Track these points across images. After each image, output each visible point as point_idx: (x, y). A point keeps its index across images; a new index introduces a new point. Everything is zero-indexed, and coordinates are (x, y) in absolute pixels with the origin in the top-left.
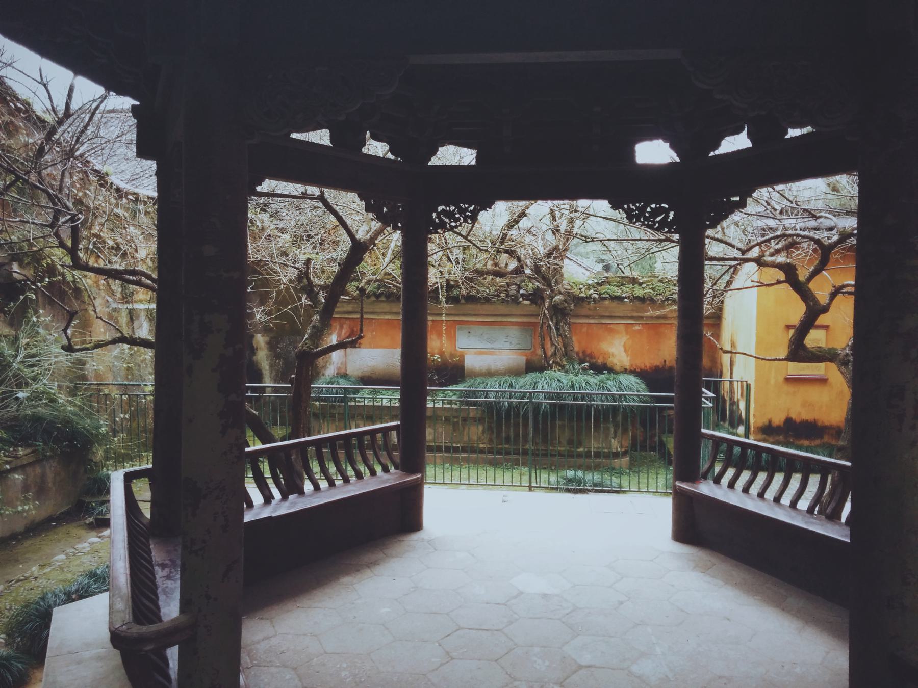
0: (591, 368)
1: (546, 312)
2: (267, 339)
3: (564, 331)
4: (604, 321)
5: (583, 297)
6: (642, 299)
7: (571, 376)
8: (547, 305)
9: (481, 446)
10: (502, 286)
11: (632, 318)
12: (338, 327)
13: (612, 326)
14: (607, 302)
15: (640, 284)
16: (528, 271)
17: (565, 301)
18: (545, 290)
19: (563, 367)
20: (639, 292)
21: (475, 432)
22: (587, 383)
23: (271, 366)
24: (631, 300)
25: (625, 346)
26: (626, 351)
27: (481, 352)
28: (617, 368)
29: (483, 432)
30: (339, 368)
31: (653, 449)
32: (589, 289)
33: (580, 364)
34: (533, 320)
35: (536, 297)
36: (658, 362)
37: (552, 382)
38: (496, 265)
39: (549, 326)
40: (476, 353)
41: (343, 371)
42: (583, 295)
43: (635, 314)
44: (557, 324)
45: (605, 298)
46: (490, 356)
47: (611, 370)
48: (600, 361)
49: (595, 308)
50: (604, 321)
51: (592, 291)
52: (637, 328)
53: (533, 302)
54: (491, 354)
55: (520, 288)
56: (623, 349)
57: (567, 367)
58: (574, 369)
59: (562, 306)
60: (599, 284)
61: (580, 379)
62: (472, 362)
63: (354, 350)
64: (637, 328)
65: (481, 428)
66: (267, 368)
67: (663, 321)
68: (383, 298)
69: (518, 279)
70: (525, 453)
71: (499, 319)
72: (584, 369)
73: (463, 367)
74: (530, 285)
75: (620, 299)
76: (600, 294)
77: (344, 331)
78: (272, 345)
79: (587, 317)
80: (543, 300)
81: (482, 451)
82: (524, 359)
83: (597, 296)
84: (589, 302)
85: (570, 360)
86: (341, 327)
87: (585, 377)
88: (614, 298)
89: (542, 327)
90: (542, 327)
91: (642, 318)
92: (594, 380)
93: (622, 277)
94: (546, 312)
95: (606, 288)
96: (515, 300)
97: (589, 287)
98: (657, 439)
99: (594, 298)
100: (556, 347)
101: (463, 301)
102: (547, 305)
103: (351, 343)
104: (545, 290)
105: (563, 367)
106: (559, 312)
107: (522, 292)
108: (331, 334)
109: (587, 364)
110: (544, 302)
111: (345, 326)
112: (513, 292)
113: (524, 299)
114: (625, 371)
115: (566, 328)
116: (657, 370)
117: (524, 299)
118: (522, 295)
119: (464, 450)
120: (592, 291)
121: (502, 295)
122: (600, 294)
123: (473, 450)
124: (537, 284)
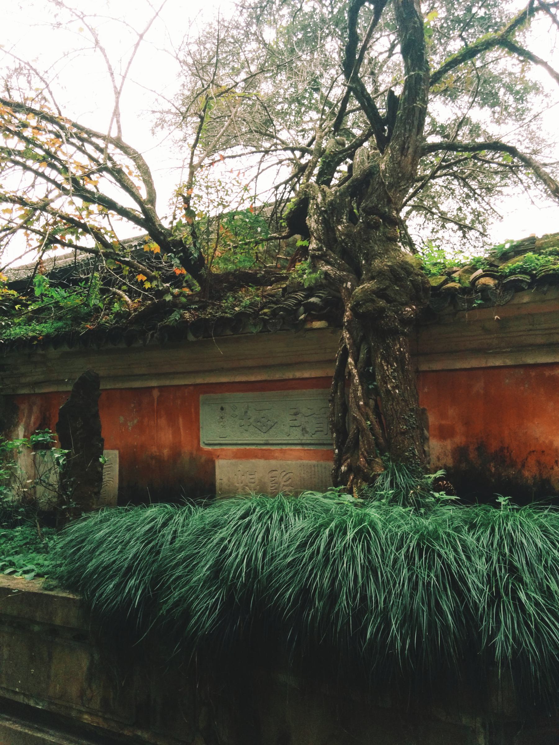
12: (26, 411)
17: (381, 293)
18: (342, 280)
46: (261, 462)
48: (529, 473)
54: (266, 455)
73: (213, 484)
77: (33, 420)
83: (490, 282)
99: (485, 287)
104: (342, 280)
108: (17, 425)
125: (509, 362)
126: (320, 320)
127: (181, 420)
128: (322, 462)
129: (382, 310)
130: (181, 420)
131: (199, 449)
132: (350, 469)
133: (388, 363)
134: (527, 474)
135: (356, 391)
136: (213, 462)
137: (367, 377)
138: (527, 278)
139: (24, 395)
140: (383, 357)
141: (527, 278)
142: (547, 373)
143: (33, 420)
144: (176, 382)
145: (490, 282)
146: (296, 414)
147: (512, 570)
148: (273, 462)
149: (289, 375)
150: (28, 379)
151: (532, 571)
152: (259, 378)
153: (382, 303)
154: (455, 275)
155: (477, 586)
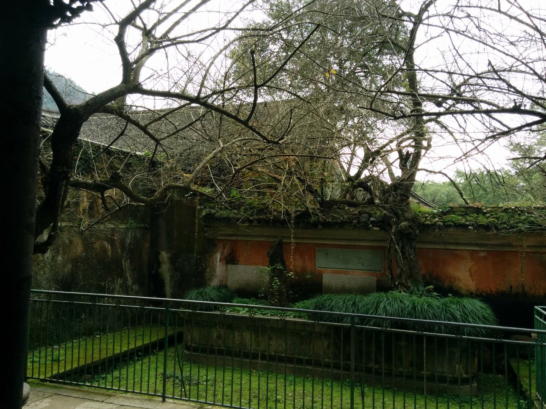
0: (435, 290)
1: (393, 237)
2: (169, 255)
3: (410, 255)
4: (449, 247)
5: (428, 225)
6: (487, 228)
7: (414, 297)
8: (393, 230)
9: (326, 360)
10: (354, 214)
11: (477, 245)
12: (222, 247)
13: (457, 252)
14: (451, 230)
15: (484, 214)
16: (377, 201)
17: (410, 227)
18: (391, 217)
19: (408, 288)
20: (482, 220)
21: (321, 347)
22: (429, 305)
23: (171, 277)
24: (475, 228)
25: (470, 271)
26: (471, 276)
27: (337, 272)
28: (464, 292)
29: (329, 347)
30: (221, 281)
31: (500, 371)
32: (434, 218)
33: (425, 286)
34: (383, 244)
35: (384, 224)
36: (504, 288)
37: (399, 302)
38: (353, 198)
39: (395, 250)
40: (332, 272)
41: (224, 283)
42: (428, 222)
43: (479, 242)
44: (403, 248)
45: (450, 226)
46: (344, 275)
47: (457, 294)
48: (446, 284)
49: (441, 235)
50: (449, 247)
51: (437, 219)
52: (482, 254)
53: (382, 228)
54: (346, 273)
55: (370, 216)
56: (468, 274)
57: (412, 288)
58: (418, 290)
59: (408, 231)
60: (444, 213)
61: (422, 301)
62: (328, 279)
63: (233, 266)
64: (482, 254)
65: (326, 343)
66: (168, 278)
67: (508, 249)
68: (256, 223)
69: (369, 208)
70: (369, 371)
71: (352, 243)
72: (429, 291)
73: (321, 284)
74: (378, 213)
75: (464, 226)
76: (444, 222)
77: (226, 251)
78: (172, 260)
79: (431, 243)
80: (390, 226)
81: (327, 366)
82: (375, 278)
83: (441, 224)
84: (434, 230)
85: (416, 282)
86: (224, 248)
87: (430, 300)
88: (459, 226)
89: (389, 251)
90: (389, 251)
91: (487, 245)
92: (437, 302)
93: (467, 208)
94: (393, 237)
95: (453, 217)
96: (365, 226)
97: (434, 216)
98: (505, 362)
99: (440, 225)
100: (402, 269)
101: (320, 227)
102: (393, 230)
103: (231, 260)
104: (391, 217)
105: (408, 288)
106: (405, 237)
107: (372, 219)
108: (216, 253)
109: (431, 287)
110: (391, 228)
111: (227, 246)
112: (363, 219)
113: (373, 226)
114: (471, 295)
115: (411, 252)
116: (502, 295)
117: (373, 226)
118: (372, 222)
119: (309, 362)
120: (437, 219)
121: (354, 221)
122: (444, 222)
123: (318, 364)
124: (385, 212)
125: (442, 247)
126: (376, 227)
127: (306, 257)
128: (371, 277)
129: (411, 233)
130: (306, 257)
131: (315, 269)
132: (399, 283)
133: (411, 249)
134: (445, 284)
135: (400, 258)
136: (322, 274)
137: (403, 253)
138: (452, 224)
139: (221, 239)
140: (410, 247)
141: (452, 224)
142: (454, 252)
143: (226, 251)
144: (305, 241)
145: (441, 224)
146: (360, 258)
147: (465, 314)
148: (349, 276)
149: (358, 243)
150: (223, 233)
151: (470, 315)
152: (344, 244)
153: (411, 230)
154: (428, 218)
155: (282, 329)
